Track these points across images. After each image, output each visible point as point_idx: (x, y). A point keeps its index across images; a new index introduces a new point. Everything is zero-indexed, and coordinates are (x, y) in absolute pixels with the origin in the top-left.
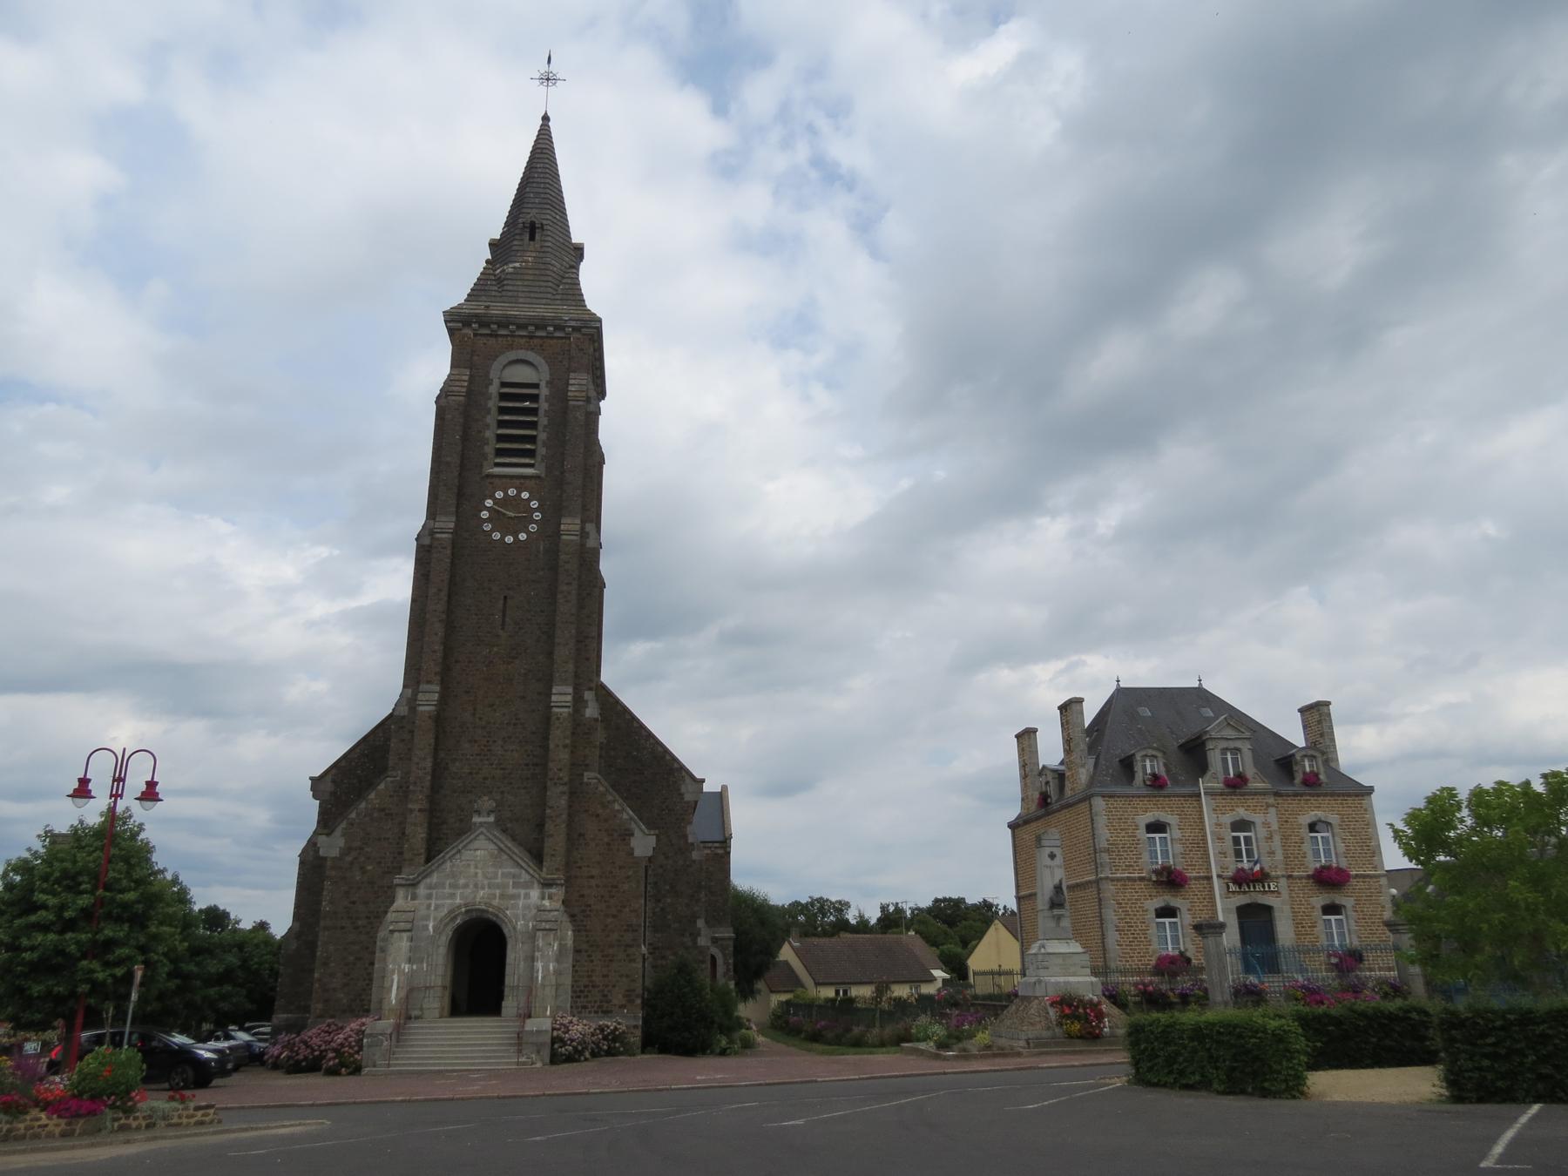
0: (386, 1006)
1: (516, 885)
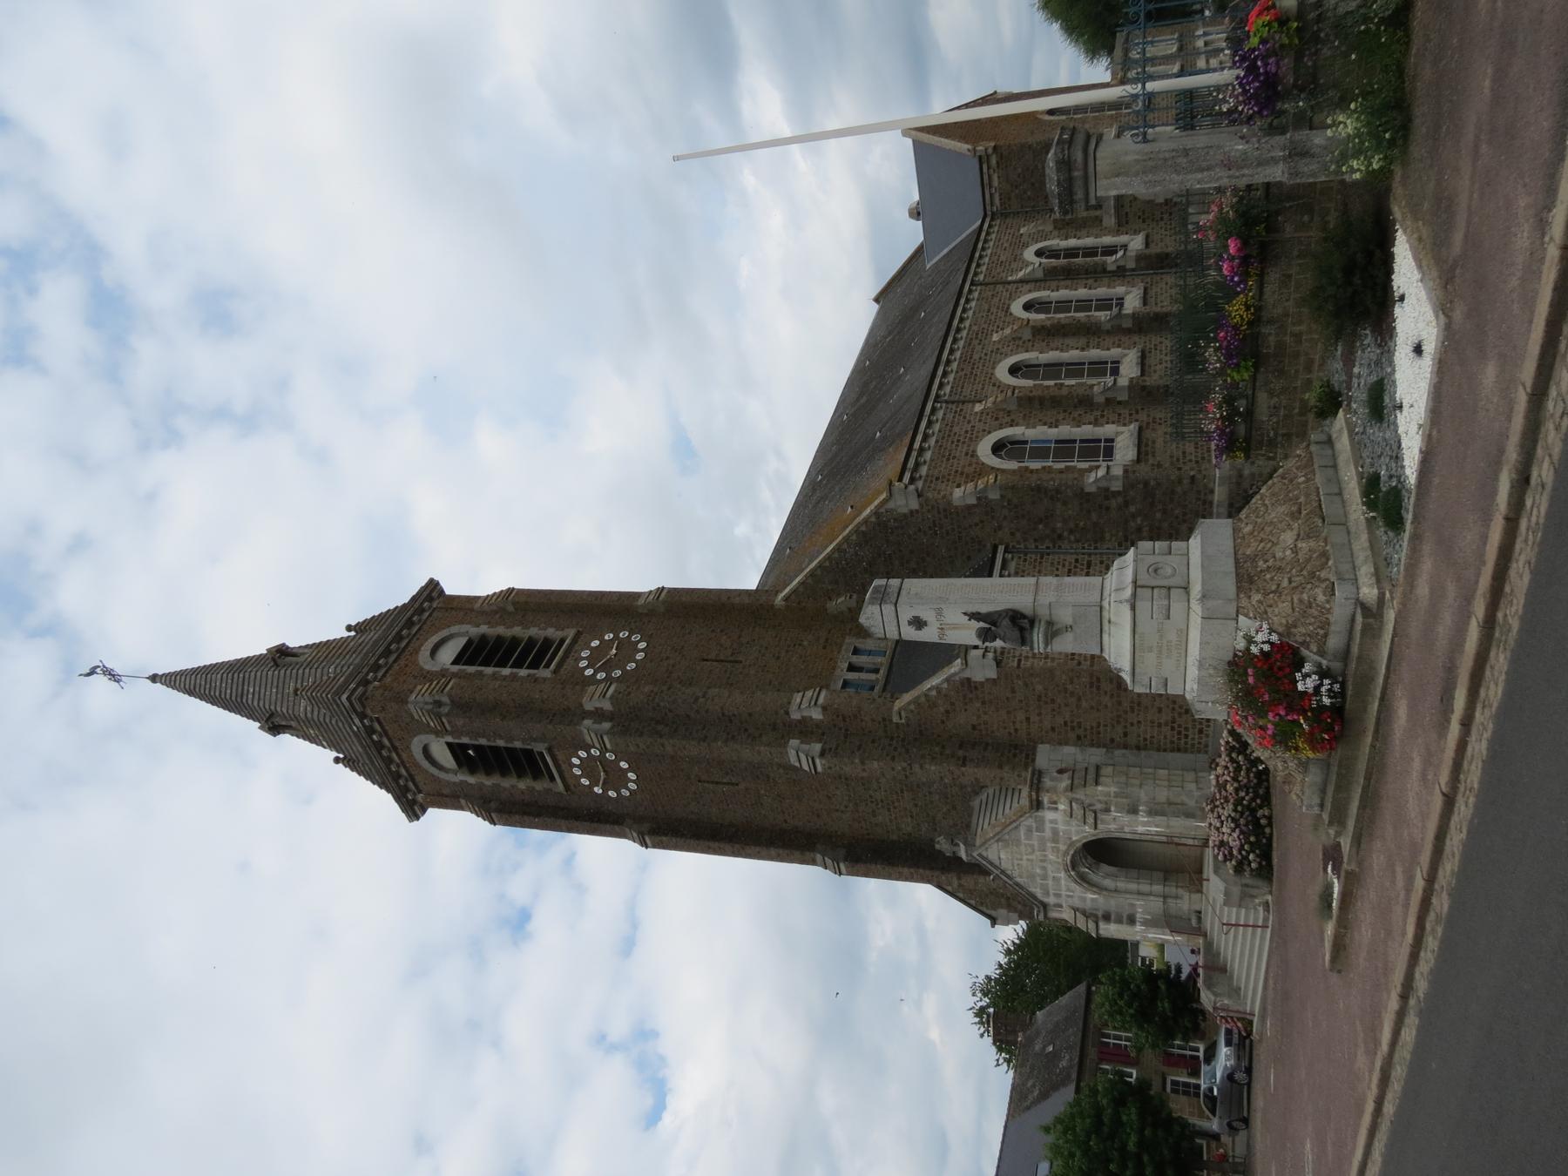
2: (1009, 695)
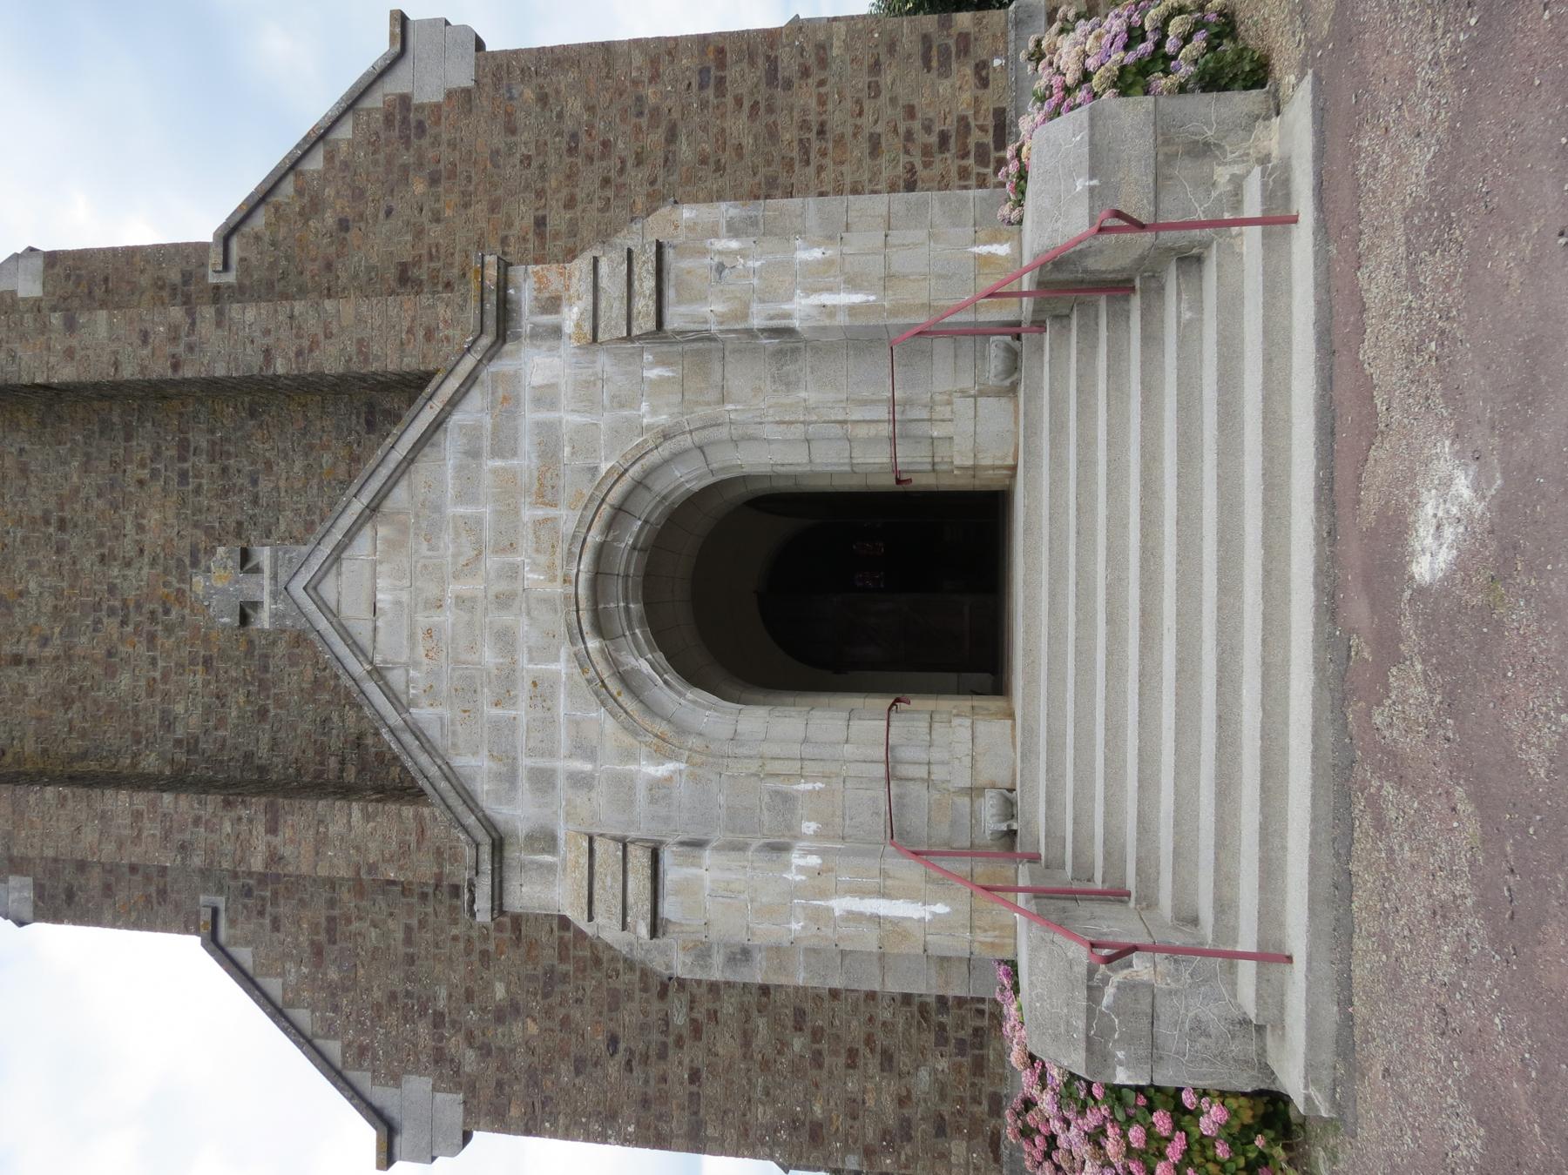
0: (957, 944)
1: (504, 445)
2: (499, 141)
